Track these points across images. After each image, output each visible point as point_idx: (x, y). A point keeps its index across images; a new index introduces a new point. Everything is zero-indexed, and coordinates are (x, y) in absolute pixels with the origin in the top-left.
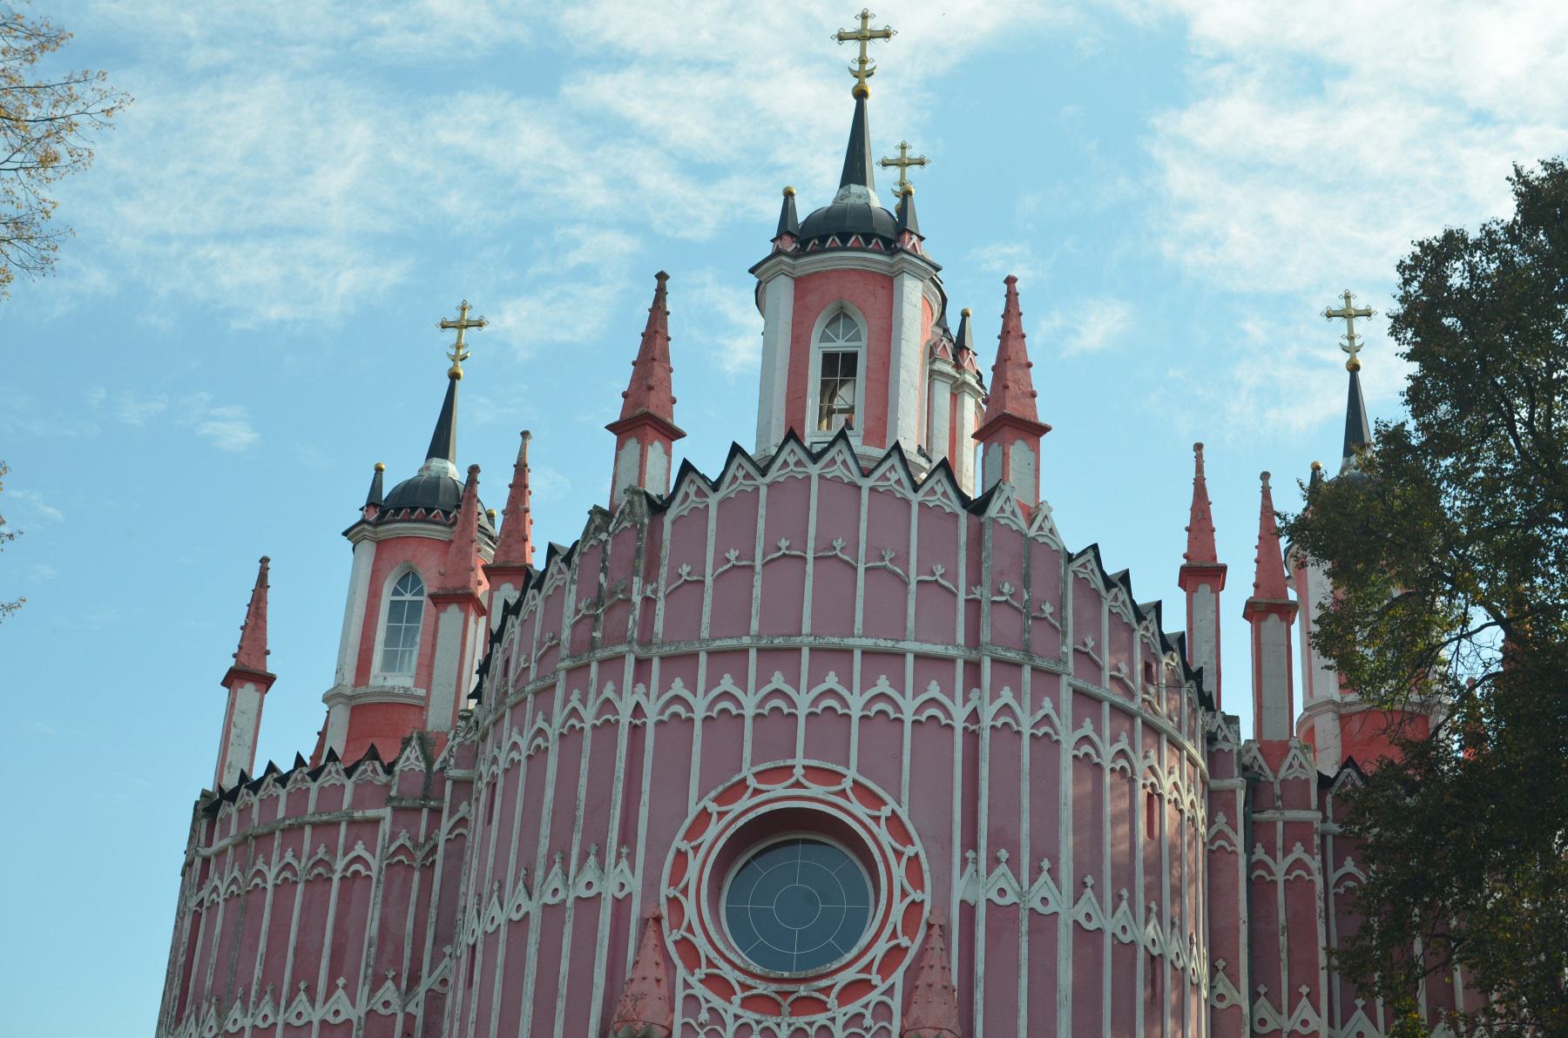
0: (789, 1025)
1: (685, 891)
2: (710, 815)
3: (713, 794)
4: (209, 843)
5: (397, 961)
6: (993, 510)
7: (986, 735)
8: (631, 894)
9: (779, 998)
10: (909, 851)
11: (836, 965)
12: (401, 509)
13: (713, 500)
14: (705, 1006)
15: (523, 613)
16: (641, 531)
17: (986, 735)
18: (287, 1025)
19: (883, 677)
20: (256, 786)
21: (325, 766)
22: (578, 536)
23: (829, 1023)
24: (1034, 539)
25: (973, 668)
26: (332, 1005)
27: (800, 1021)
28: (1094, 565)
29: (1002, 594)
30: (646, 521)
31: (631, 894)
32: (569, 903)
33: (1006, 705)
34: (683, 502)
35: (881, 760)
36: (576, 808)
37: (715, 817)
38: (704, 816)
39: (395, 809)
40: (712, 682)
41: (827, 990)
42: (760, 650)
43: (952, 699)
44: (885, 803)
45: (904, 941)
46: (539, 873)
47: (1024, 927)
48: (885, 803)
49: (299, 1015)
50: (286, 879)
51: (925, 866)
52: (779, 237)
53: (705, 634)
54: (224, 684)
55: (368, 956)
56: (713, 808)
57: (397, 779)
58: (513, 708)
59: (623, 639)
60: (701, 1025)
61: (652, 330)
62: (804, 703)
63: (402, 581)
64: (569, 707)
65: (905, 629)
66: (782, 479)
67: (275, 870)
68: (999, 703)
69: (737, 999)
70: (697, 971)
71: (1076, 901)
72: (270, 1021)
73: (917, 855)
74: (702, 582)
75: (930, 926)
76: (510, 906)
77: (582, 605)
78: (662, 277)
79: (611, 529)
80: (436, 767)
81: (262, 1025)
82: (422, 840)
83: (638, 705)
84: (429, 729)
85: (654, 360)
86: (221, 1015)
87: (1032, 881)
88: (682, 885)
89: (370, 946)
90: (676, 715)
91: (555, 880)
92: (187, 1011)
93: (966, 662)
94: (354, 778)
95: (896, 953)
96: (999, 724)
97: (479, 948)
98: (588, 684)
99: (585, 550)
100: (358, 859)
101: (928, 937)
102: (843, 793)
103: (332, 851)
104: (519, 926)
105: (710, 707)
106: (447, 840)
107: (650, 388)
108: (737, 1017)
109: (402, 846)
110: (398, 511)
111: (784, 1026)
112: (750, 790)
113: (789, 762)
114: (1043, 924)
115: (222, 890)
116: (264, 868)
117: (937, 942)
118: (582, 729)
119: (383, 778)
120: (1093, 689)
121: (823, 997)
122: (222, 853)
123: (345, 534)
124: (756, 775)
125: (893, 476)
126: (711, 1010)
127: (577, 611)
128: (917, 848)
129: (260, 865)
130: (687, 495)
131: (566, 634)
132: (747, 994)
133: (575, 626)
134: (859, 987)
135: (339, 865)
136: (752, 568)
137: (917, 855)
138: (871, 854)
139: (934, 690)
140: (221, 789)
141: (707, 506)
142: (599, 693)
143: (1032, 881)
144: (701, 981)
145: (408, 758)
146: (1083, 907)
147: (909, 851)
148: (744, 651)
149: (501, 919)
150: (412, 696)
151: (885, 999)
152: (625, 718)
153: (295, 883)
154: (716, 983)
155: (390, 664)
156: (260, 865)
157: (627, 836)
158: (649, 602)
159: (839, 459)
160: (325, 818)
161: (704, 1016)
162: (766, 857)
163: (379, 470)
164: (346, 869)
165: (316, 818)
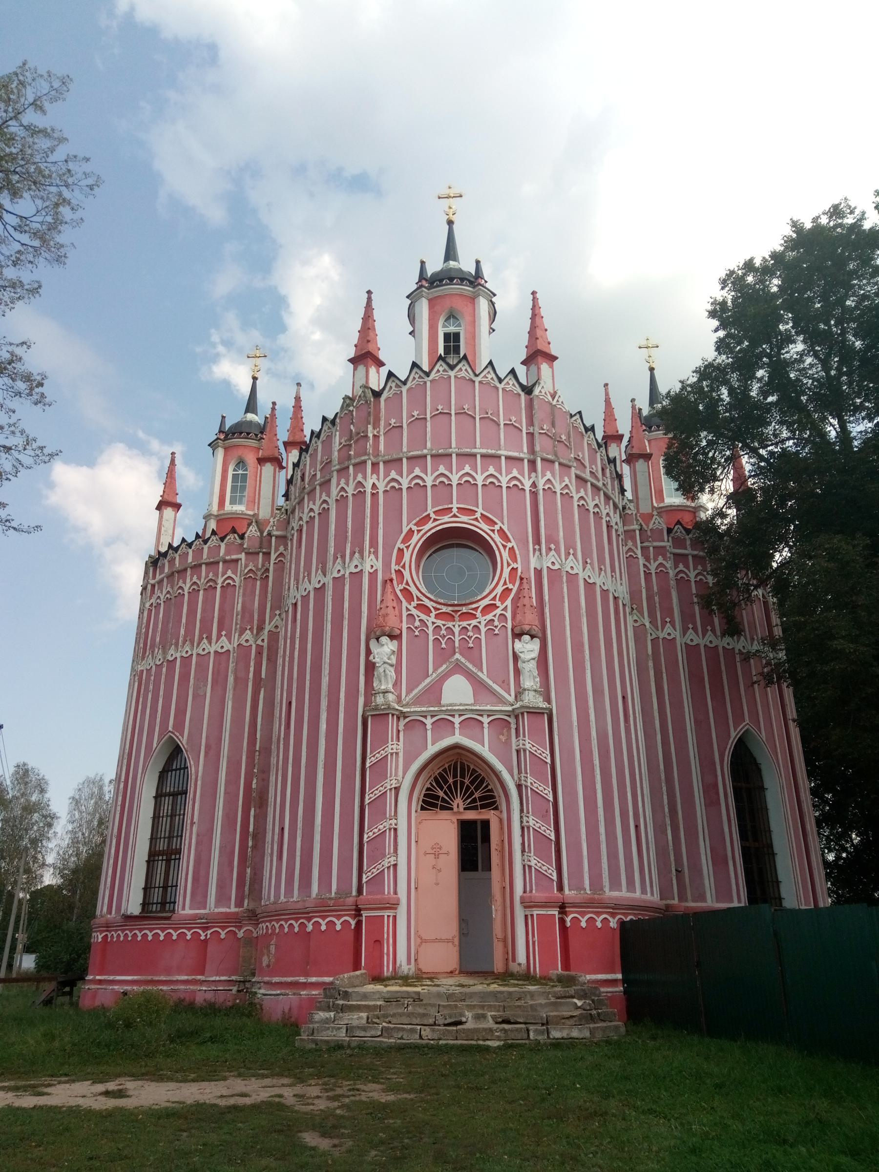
0: (459, 626)
1: (404, 567)
2: (413, 531)
3: (414, 522)
4: (154, 577)
5: (251, 621)
6: (536, 391)
7: (541, 492)
8: (377, 570)
9: (453, 614)
10: (509, 545)
11: (479, 598)
12: (235, 433)
13: (404, 389)
14: (417, 619)
15: (301, 466)
16: (370, 404)
17: (541, 492)
18: (198, 654)
19: (491, 467)
20: (176, 549)
21: (209, 538)
22: (338, 410)
23: (478, 624)
24: (555, 405)
25: (532, 463)
26: (219, 644)
27: (464, 624)
28: (579, 421)
29: (543, 429)
30: (372, 400)
31: (377, 570)
32: (347, 575)
33: (549, 480)
34: (389, 391)
35: (494, 504)
36: (347, 532)
37: (416, 532)
38: (411, 532)
39: (246, 553)
40: (410, 471)
41: (476, 609)
42: (432, 456)
43: (524, 477)
44: (496, 524)
45: (510, 586)
46: (330, 564)
47: (565, 578)
48: (496, 524)
49: (204, 649)
50: (194, 589)
51: (517, 552)
52: (420, 281)
53: (405, 450)
54: (157, 509)
55: (236, 620)
56: (415, 528)
57: (246, 540)
58: (308, 494)
59: (365, 454)
60: (416, 628)
61: (367, 316)
62: (455, 479)
63: (238, 465)
64: (340, 487)
65: (500, 445)
66: (437, 378)
67: (188, 585)
68: (545, 478)
69: (433, 615)
70: (412, 603)
71: (584, 570)
72: (190, 653)
73: (513, 547)
74: (402, 427)
75: (521, 579)
76: (314, 581)
77: (343, 441)
78: (369, 292)
79: (355, 404)
80: (265, 534)
81: (185, 656)
82: (260, 566)
83: (374, 484)
84: (260, 518)
85: (369, 329)
86: (165, 653)
87: (566, 559)
88: (402, 564)
89: (237, 615)
90: (393, 487)
91: (338, 567)
92: (147, 654)
93: (529, 461)
94: (225, 542)
95: (507, 591)
96: (546, 488)
97: (299, 604)
98: (349, 476)
99: (342, 416)
100: (229, 578)
101: (521, 584)
102: (476, 519)
103: (216, 575)
104: (320, 591)
105: (410, 482)
106: (275, 563)
107: (368, 341)
108: (433, 623)
109: (251, 570)
110: (234, 434)
111: (457, 626)
112: (432, 519)
113: (450, 506)
114: (572, 578)
115: (162, 597)
116: (183, 585)
117: (525, 586)
118: (347, 496)
119: (239, 541)
120: (583, 475)
121: (474, 612)
122: (161, 582)
123: (209, 445)
124: (435, 512)
125: (490, 376)
126: (421, 620)
127: (340, 444)
128: (513, 544)
129: (181, 584)
130: (391, 387)
131: (336, 454)
132: (437, 612)
133: (339, 450)
134: (491, 607)
135: (220, 581)
136: (425, 419)
137: (513, 547)
138: (492, 547)
139: (515, 473)
140: (159, 552)
141: (402, 392)
142: (355, 479)
143: (566, 559)
144: (414, 607)
145: (251, 531)
146: (588, 571)
147: (509, 545)
148: (425, 456)
149: (310, 588)
150: (246, 514)
151: (503, 612)
152: (369, 490)
153: (199, 590)
154: (421, 607)
155: (233, 502)
156: (181, 584)
157: (374, 543)
158: (376, 437)
159: (464, 369)
160: (212, 560)
161: (417, 623)
162: (439, 553)
163: (223, 417)
164: (223, 582)
165: (208, 561)
